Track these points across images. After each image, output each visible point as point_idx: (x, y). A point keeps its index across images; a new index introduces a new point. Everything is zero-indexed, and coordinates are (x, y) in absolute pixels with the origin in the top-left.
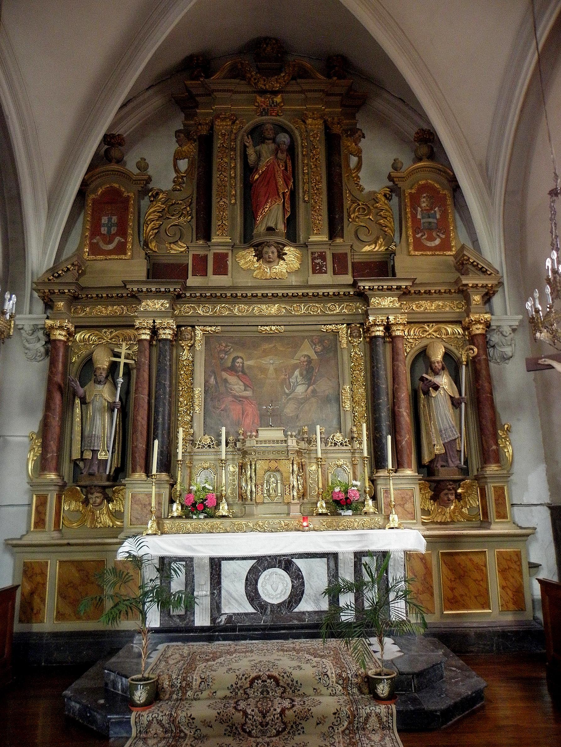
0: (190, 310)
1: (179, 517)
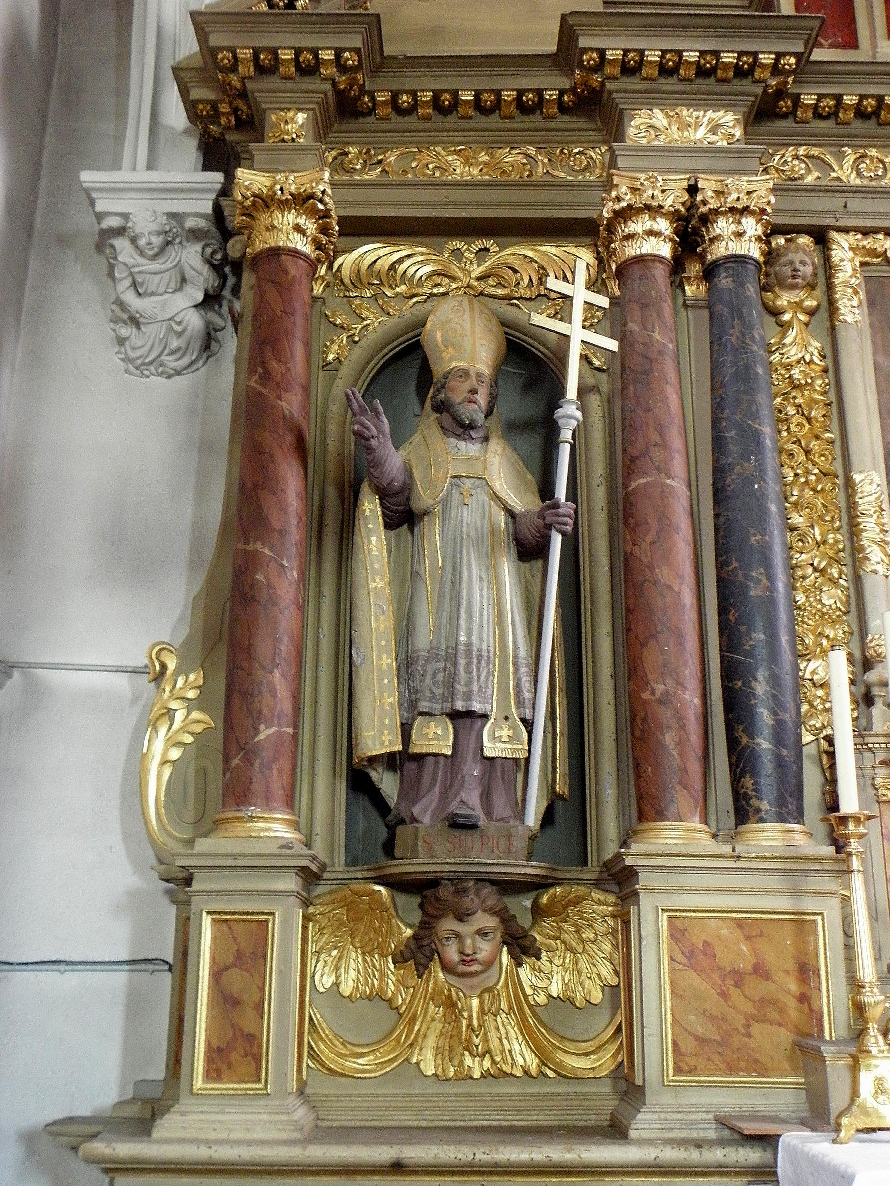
0: (809, 171)
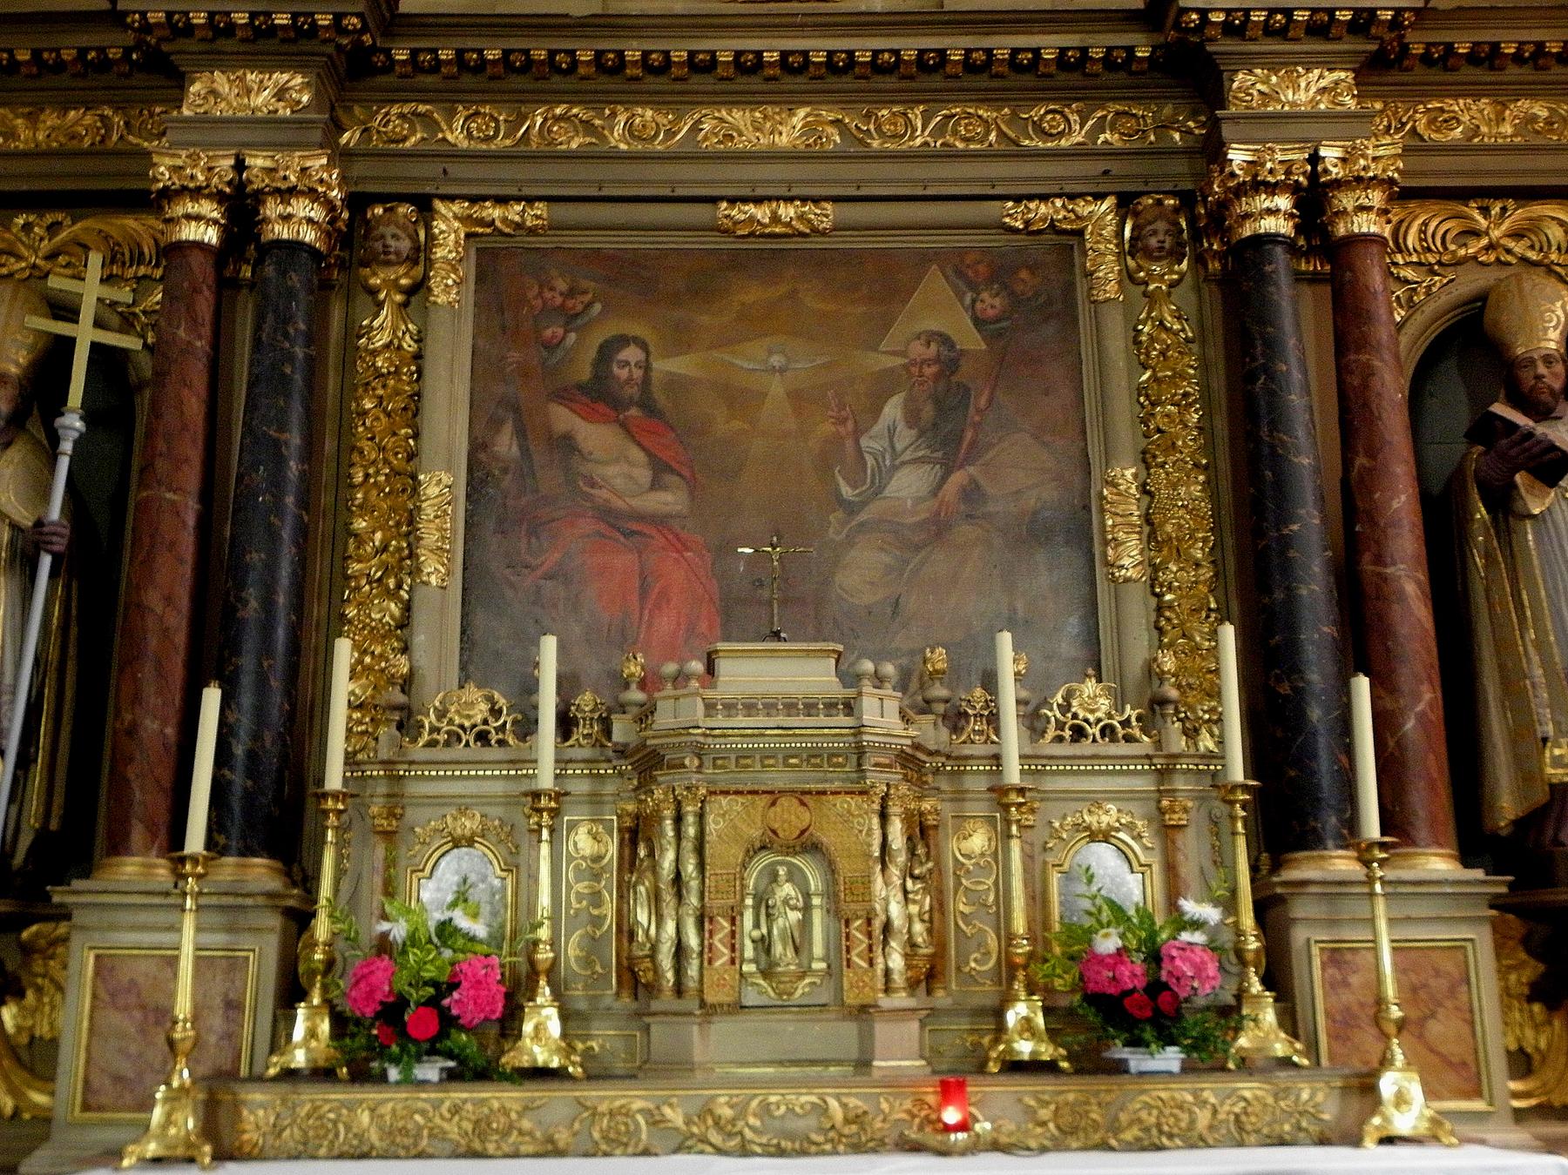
0: (413, 131)
1: (321, 1074)
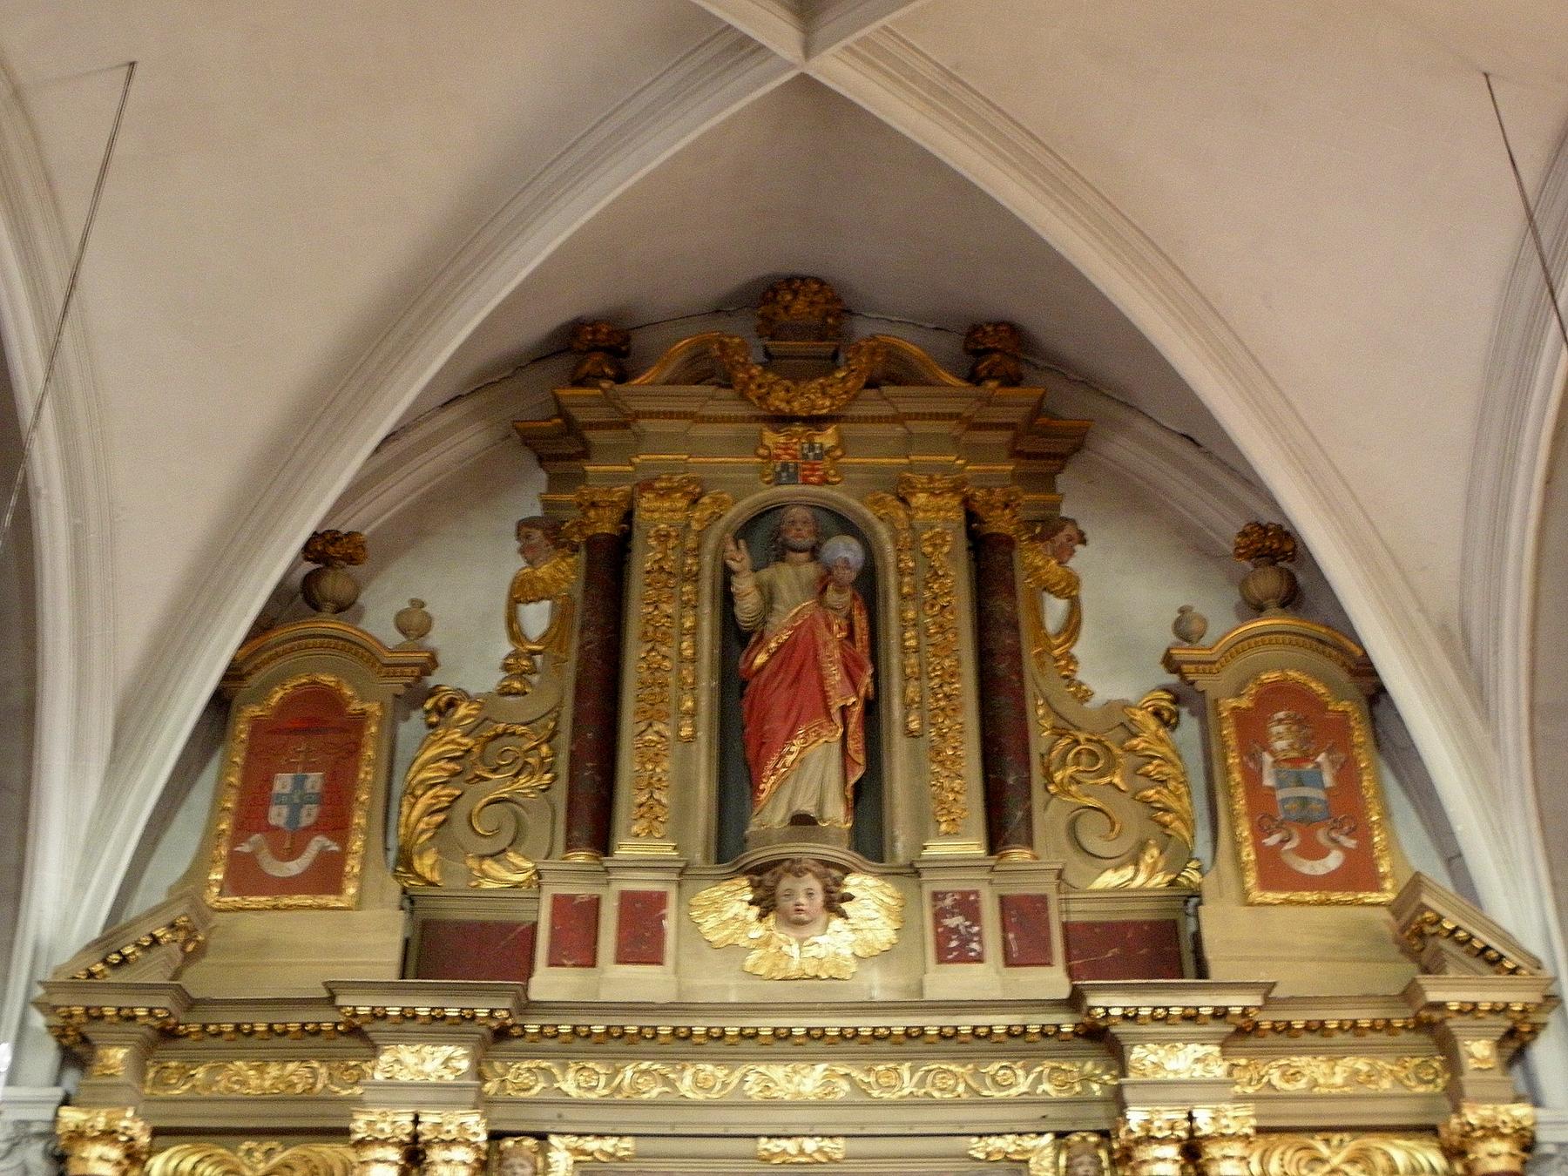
0: (537, 1081)
